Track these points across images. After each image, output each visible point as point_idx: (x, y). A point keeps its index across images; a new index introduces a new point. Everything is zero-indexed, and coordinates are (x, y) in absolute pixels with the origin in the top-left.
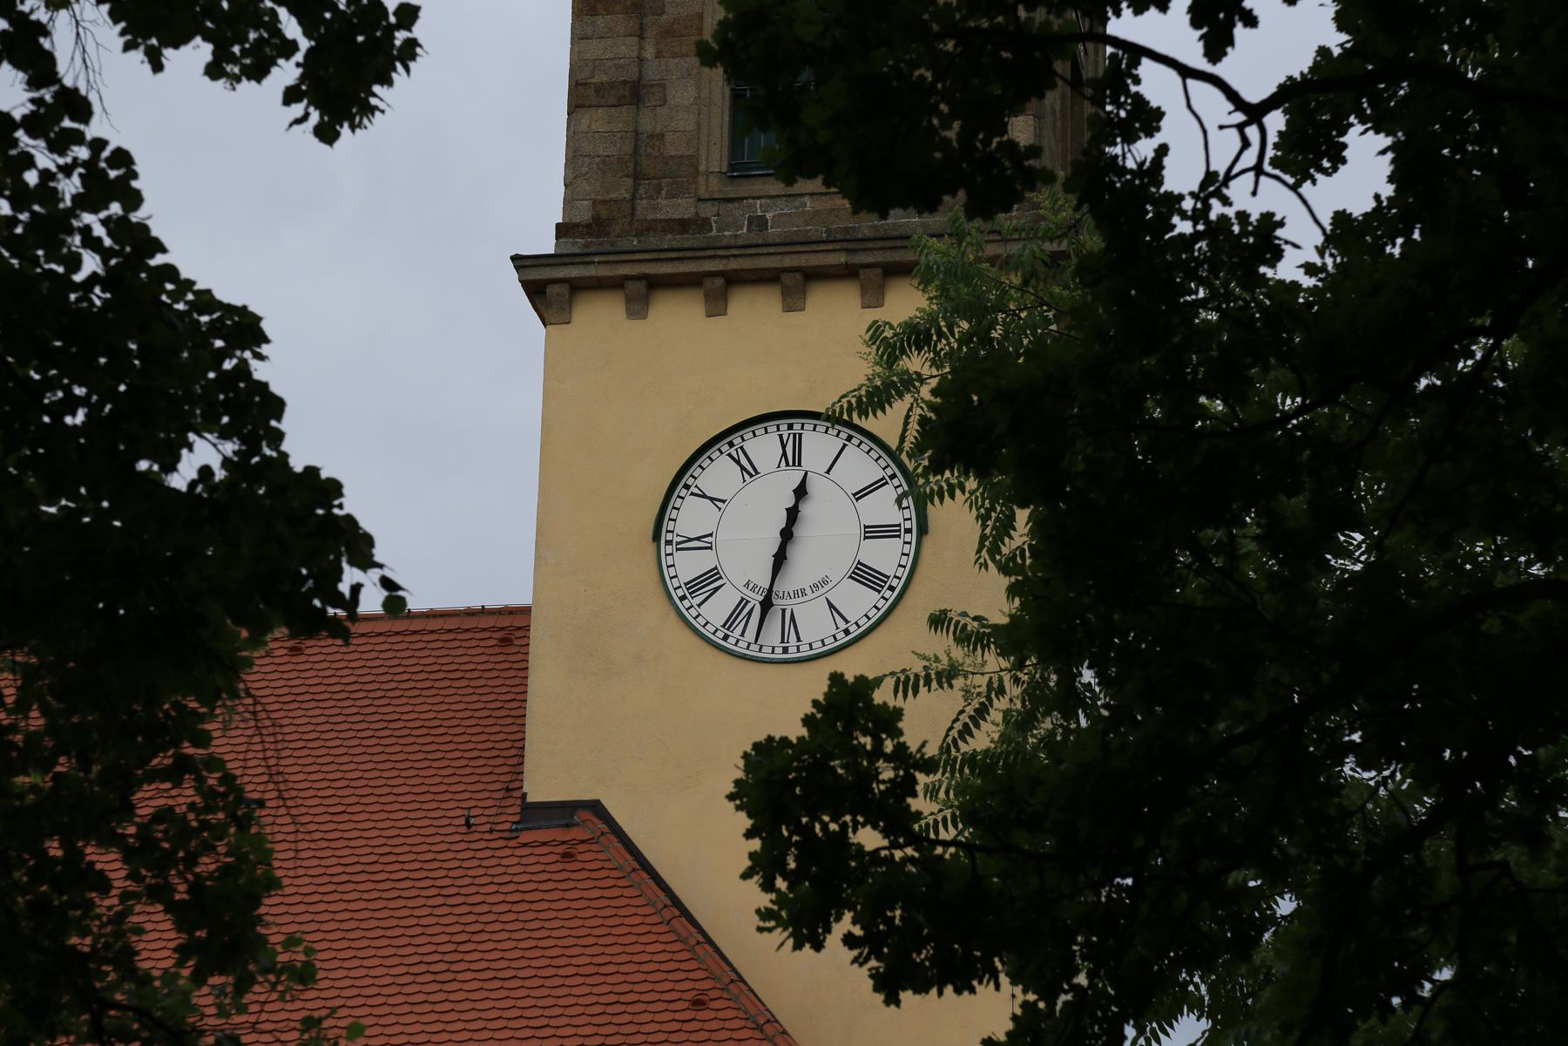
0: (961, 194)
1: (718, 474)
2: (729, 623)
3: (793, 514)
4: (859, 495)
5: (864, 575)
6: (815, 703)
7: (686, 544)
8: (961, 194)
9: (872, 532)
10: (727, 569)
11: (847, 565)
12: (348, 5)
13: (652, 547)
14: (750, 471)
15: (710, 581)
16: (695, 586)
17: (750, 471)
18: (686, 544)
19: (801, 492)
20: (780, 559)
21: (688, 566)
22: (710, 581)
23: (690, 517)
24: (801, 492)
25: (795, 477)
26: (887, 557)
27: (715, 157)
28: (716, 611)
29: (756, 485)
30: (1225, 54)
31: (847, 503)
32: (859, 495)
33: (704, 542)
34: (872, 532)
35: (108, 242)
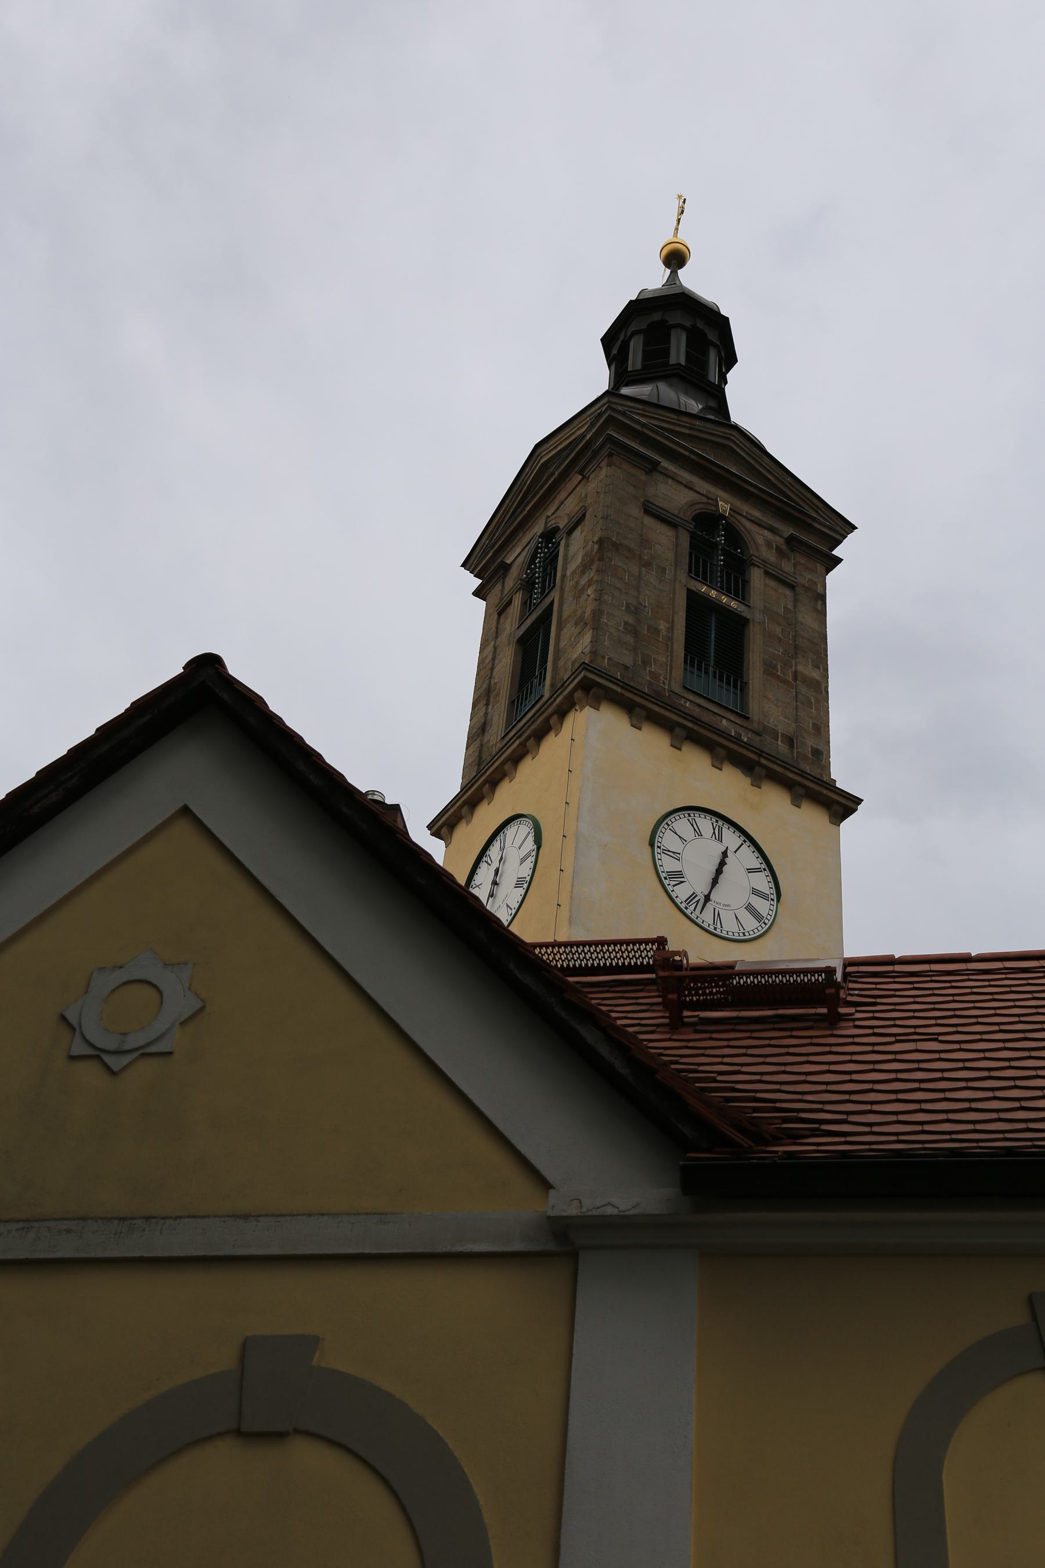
3: (722, 863)
4: (750, 871)
7: (667, 851)
10: (687, 873)
13: (649, 849)
15: (678, 876)
19: (725, 854)
23: (668, 840)
24: (725, 854)
26: (763, 907)
27: (678, 673)
29: (700, 841)
31: (744, 873)
32: (750, 871)
33: (676, 856)
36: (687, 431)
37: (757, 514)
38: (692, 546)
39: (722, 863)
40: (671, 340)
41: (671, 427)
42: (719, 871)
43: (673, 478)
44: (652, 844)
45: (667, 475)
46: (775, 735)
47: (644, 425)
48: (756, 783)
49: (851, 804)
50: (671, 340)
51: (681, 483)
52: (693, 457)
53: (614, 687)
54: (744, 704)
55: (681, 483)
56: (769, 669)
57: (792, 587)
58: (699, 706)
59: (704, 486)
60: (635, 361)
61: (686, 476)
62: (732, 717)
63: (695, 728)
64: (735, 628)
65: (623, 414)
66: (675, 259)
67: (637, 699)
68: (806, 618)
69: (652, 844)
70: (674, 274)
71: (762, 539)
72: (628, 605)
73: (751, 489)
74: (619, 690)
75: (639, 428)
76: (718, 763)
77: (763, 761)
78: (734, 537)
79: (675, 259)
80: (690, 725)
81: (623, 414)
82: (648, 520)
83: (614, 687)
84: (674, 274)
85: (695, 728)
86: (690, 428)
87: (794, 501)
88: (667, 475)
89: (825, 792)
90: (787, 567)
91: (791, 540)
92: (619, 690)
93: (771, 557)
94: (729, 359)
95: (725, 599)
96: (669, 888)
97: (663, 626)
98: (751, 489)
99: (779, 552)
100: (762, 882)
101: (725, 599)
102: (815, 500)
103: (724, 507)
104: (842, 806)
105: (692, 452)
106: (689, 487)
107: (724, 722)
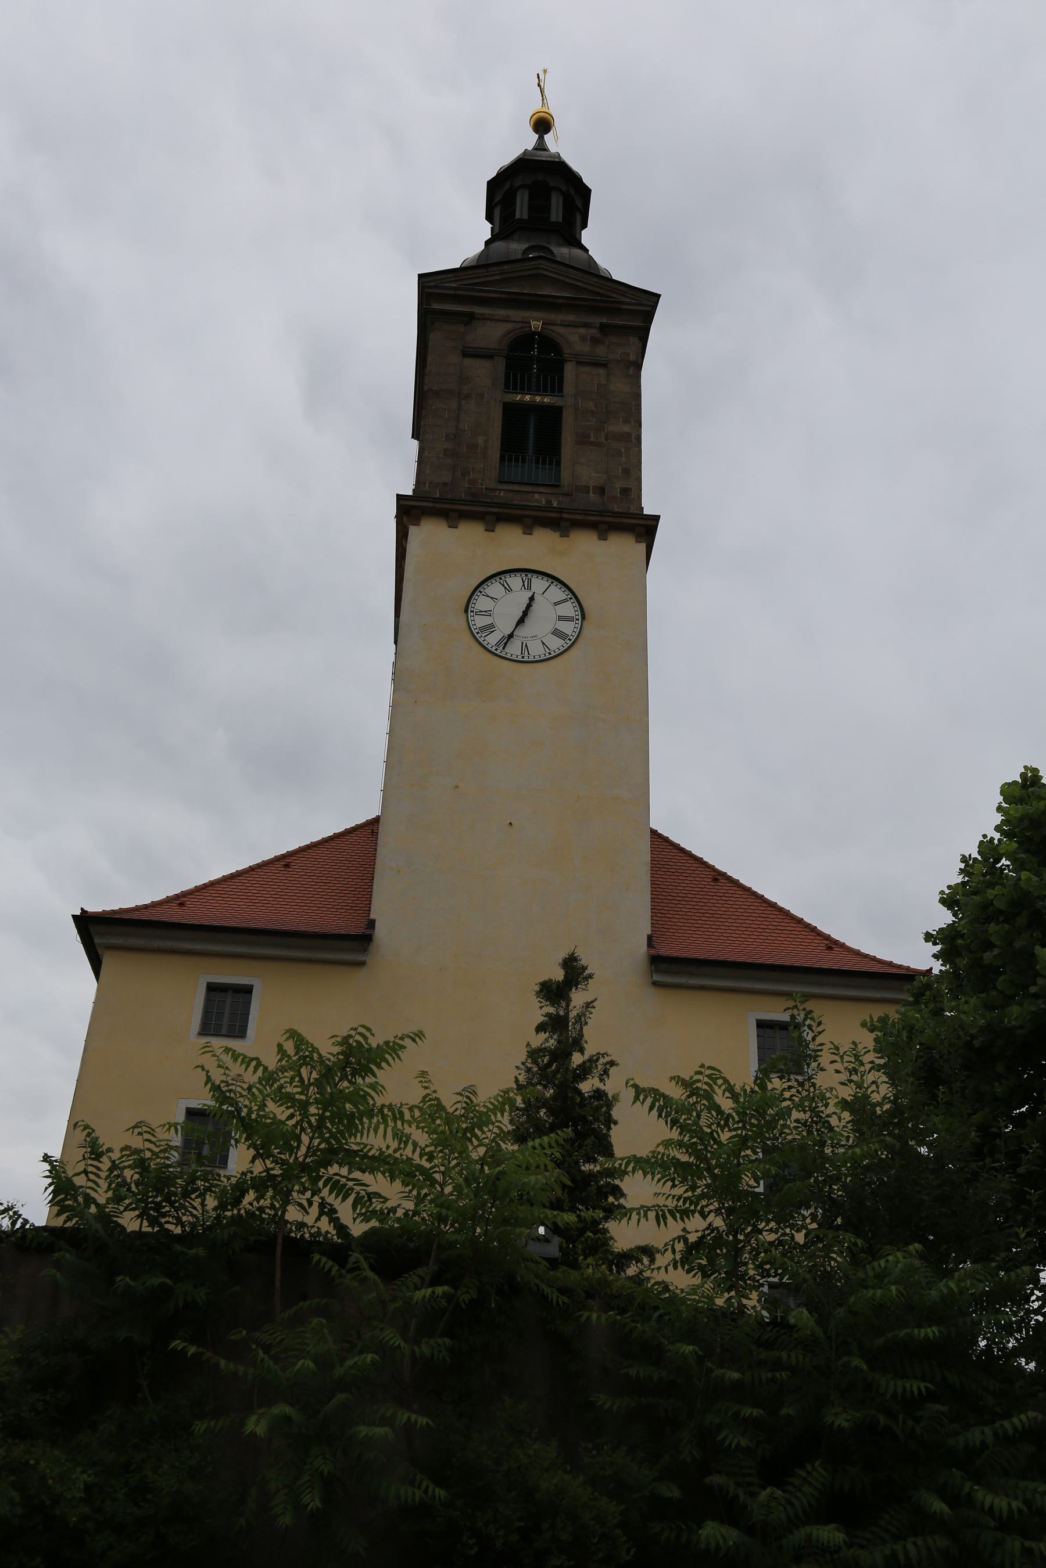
0: (937, 967)
1: (495, 589)
2: (498, 644)
3: (529, 606)
4: (556, 604)
5: (556, 633)
6: (999, 809)
7: (480, 613)
8: (937, 967)
9: (561, 618)
11: (551, 628)
12: (1045, 1341)
13: (464, 616)
14: (508, 589)
15: (490, 628)
16: (483, 629)
17: (508, 589)
18: (480, 613)
19: (532, 599)
20: (521, 621)
21: (480, 621)
22: (490, 628)
23: (481, 603)
24: (532, 599)
25: (530, 594)
26: (568, 628)
28: (492, 640)
29: (512, 594)
30: (489, 217)
32: (556, 604)
33: (488, 613)
34: (561, 618)
35: (63, 1196)
36: (499, 277)
37: (571, 318)
38: (508, 367)
39: (529, 606)
40: (538, 196)
41: (484, 280)
42: (525, 613)
43: (491, 320)
44: (466, 611)
45: (484, 318)
46: (587, 489)
47: (456, 289)
48: (565, 534)
49: (654, 523)
50: (538, 196)
51: (499, 320)
52: (503, 296)
53: (426, 504)
54: (558, 477)
55: (499, 320)
56: (582, 440)
57: (604, 366)
58: (512, 491)
59: (517, 315)
60: (521, 211)
61: (502, 312)
62: (542, 490)
63: (501, 510)
64: (552, 417)
65: (436, 287)
66: (542, 125)
67: (448, 506)
68: (619, 386)
69: (466, 611)
70: (541, 139)
71: (574, 339)
72: (447, 436)
73: (560, 301)
74: (431, 505)
75: (452, 292)
76: (528, 531)
77: (565, 516)
78: (548, 343)
79: (542, 125)
80: (495, 510)
81: (436, 287)
82: (467, 362)
83: (426, 504)
84: (541, 139)
85: (501, 510)
86: (501, 274)
87: (602, 295)
88: (484, 318)
89: (625, 521)
90: (601, 351)
91: (604, 328)
92: (431, 505)
93: (585, 348)
94: (585, 225)
95: (538, 399)
96: (481, 640)
97: (480, 440)
98: (560, 301)
99: (595, 341)
100: (569, 609)
101: (538, 399)
102: (617, 286)
103: (536, 325)
104: (646, 529)
105: (501, 292)
106: (507, 320)
107: (536, 496)
